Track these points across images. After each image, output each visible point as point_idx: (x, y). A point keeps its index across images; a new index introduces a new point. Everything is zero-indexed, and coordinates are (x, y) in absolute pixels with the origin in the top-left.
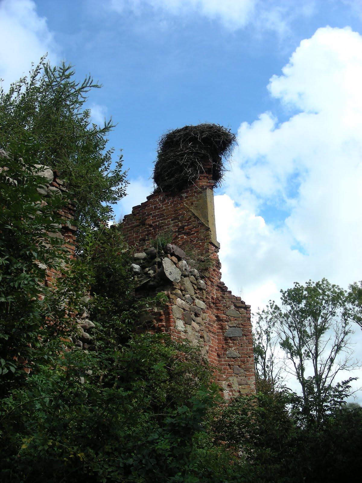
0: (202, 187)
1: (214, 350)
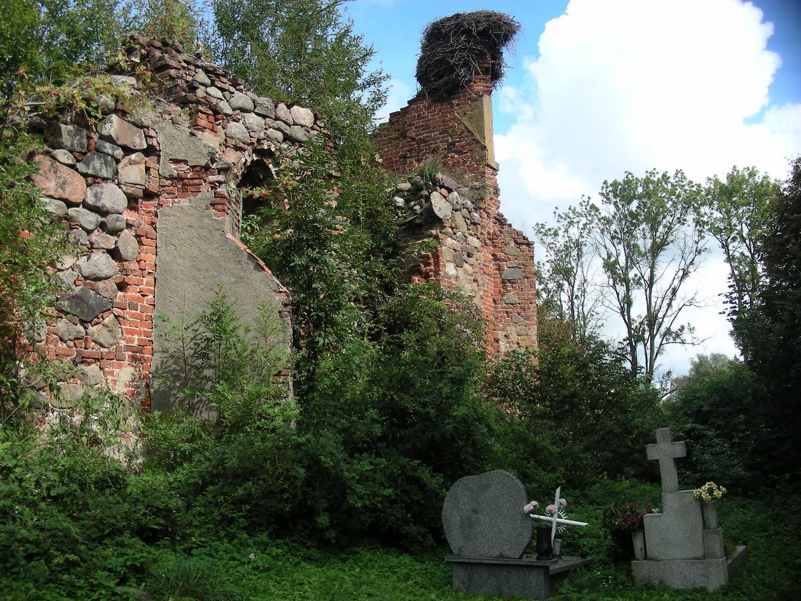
0: (477, 93)
1: (490, 295)
